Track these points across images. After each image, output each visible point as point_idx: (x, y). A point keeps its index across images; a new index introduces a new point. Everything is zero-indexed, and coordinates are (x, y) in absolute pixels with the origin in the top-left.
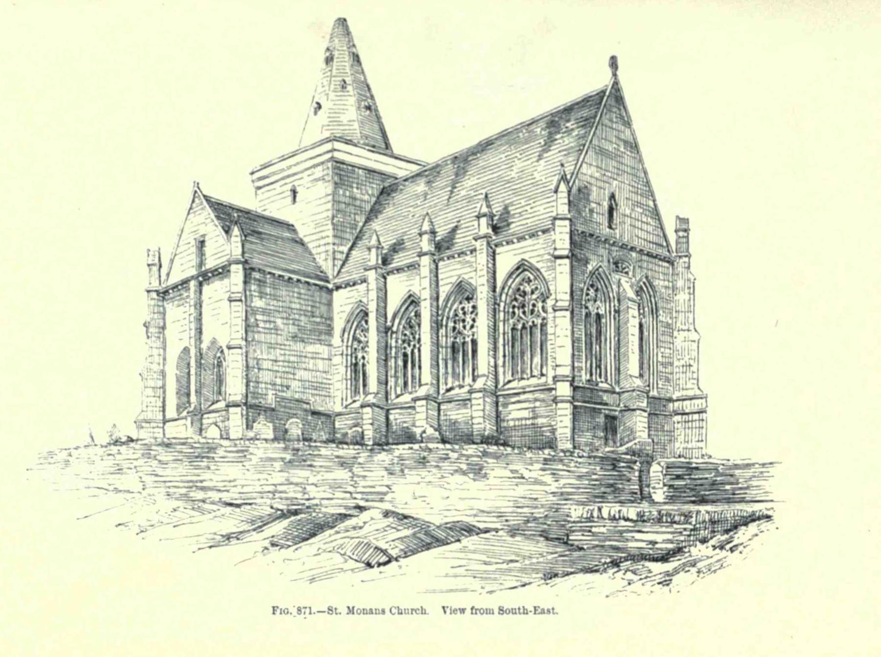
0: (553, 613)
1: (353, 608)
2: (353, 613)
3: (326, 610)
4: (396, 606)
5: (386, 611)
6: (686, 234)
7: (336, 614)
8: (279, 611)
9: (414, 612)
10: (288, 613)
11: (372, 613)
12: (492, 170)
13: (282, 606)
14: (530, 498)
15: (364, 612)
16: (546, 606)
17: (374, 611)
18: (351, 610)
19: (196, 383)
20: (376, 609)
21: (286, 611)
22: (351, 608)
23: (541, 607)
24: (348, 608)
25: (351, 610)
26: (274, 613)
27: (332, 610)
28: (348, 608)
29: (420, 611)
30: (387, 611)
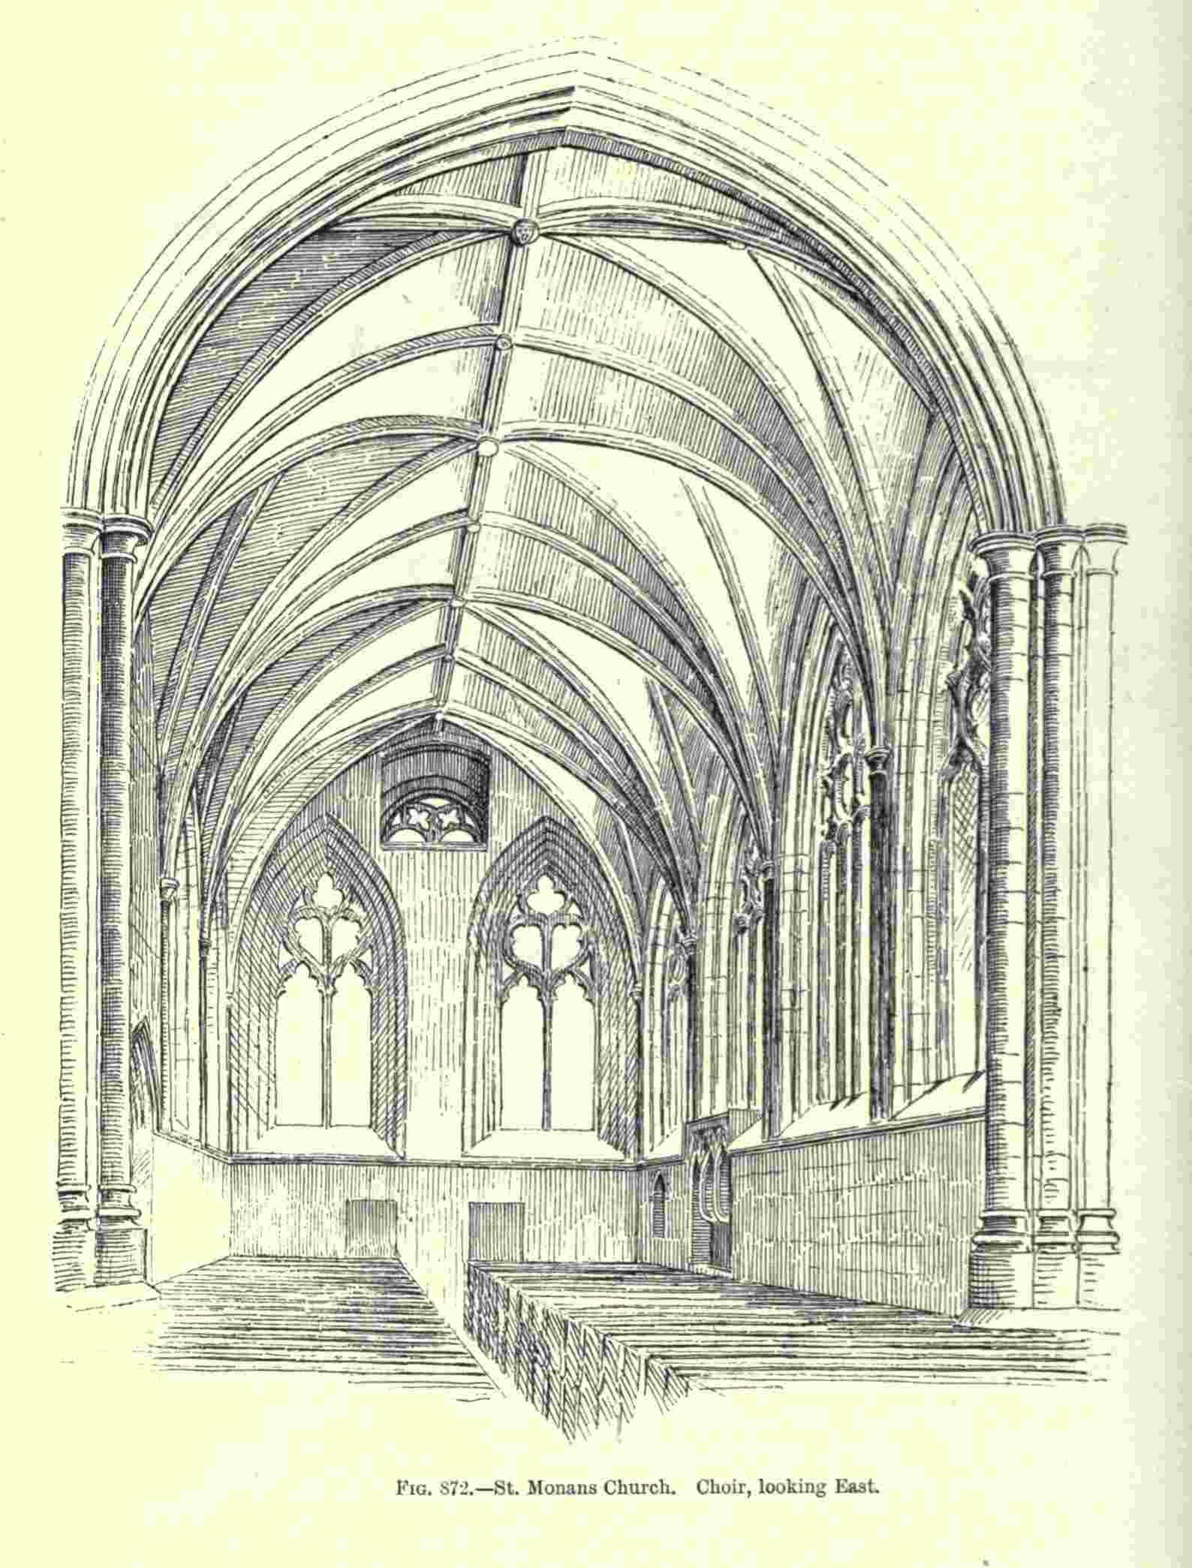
0: (510, 1493)
1: (540, 1482)
2: (540, 1493)
3: (493, 1486)
4: (709, 1478)
5: (597, 1488)
6: (499, 198)
7: (871, 1491)
8: (408, 1488)
9: (647, 1490)
10: (424, 1491)
11: (573, 1493)
12: (141, 467)
13: (414, 1481)
14: (429, 1323)
15: (558, 1489)
16: (857, 1479)
17: (576, 1489)
18: (535, 1487)
19: (702, 1026)
20: (580, 1486)
21: (421, 1489)
22: (536, 1483)
23: (849, 1482)
24: (531, 1482)
25: (535, 1487)
26: (399, 1493)
27: (503, 1488)
28: (531, 1482)
29: (659, 1487)
30: (600, 1490)
